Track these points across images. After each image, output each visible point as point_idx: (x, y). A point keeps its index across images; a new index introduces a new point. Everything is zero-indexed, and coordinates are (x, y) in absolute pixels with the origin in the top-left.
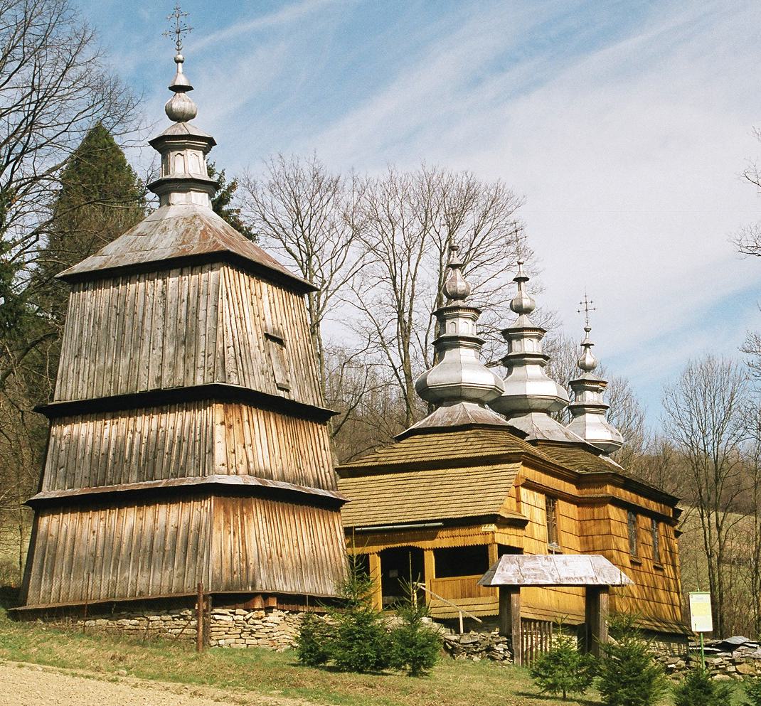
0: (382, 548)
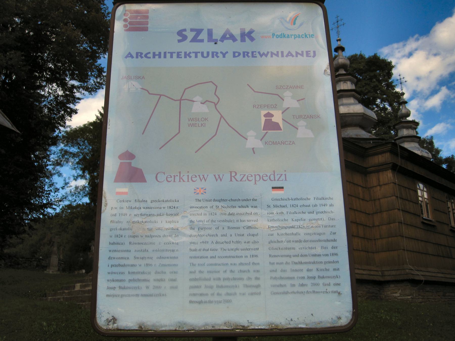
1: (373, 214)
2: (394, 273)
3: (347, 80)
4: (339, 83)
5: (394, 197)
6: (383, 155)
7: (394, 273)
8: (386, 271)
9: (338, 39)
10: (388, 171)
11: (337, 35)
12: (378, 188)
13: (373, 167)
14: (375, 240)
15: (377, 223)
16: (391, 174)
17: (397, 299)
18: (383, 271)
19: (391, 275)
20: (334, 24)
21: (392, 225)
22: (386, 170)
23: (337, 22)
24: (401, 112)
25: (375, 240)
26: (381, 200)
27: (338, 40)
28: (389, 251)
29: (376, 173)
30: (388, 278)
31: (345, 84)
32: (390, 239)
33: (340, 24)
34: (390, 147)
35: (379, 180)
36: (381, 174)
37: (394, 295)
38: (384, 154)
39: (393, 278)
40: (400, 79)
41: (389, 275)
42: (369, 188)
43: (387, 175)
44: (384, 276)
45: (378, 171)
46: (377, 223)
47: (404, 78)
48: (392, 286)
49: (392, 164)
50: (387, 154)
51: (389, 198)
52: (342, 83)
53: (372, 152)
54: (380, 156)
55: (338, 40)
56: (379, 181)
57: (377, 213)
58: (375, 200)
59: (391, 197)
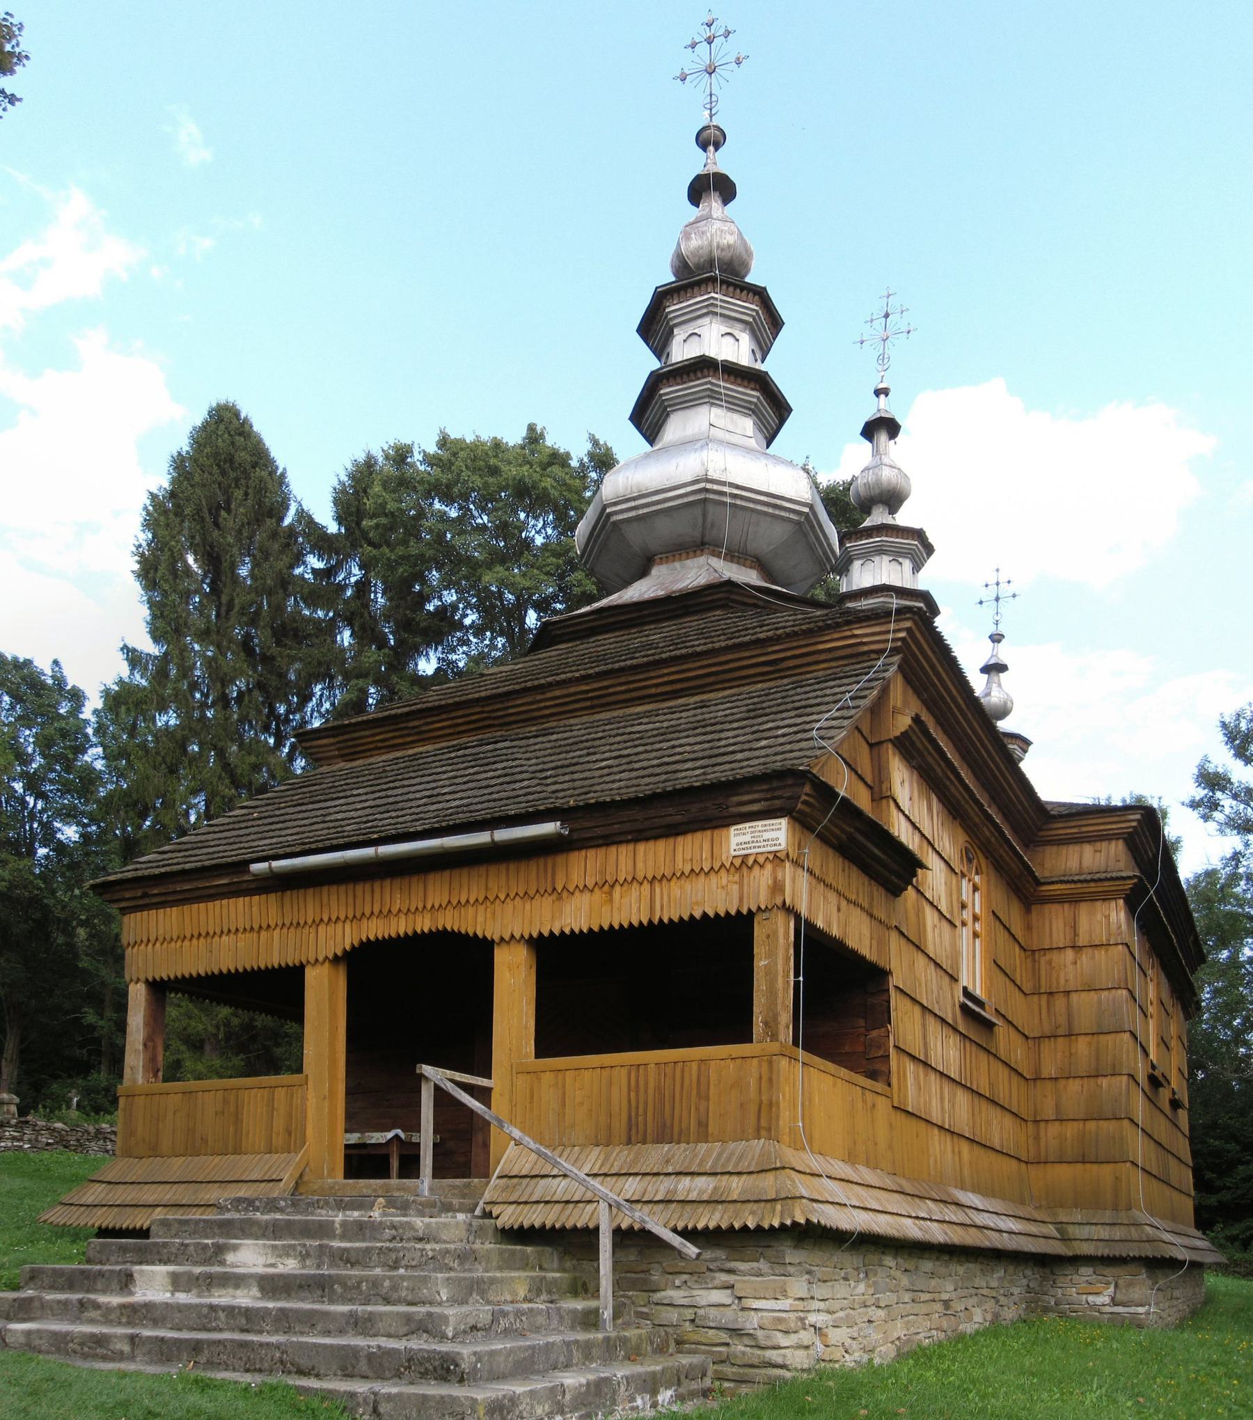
0: (347, 937)
1: (1039, 1038)
2: (1104, 1233)
3: (904, 555)
4: (877, 559)
5: (1125, 992)
6: (1098, 844)
7: (1104, 1233)
8: (1073, 1223)
9: (881, 386)
10: (1113, 904)
11: (880, 368)
12: (1070, 954)
13: (1061, 882)
14: (1036, 1122)
15: (1049, 1070)
16: (1122, 915)
17: (1099, 1311)
18: (1061, 1223)
19: (1092, 1240)
20: (872, 321)
21: (1104, 1082)
22: (1106, 897)
23: (887, 316)
24: (988, 698)
25: (1036, 1122)
26: (1074, 997)
27: (878, 393)
28: (1084, 1162)
29: (1066, 906)
30: (1086, 1249)
31: (895, 565)
32: (1091, 1125)
33: (896, 327)
34: (1134, 824)
35: (1075, 928)
36: (1084, 908)
37: (1091, 1298)
38: (1105, 844)
39: (1103, 1250)
40: (998, 584)
41: (1087, 1240)
42: (1033, 951)
43: (1108, 917)
44: (1070, 1240)
45: (1074, 900)
46: (1049, 1070)
47: (1009, 582)
48: (1086, 1271)
49: (1136, 880)
50: (1113, 843)
51: (1106, 993)
52: (886, 558)
53: (1061, 832)
54: (1088, 850)
55: (878, 393)
56: (1076, 934)
57: (1055, 1036)
58: (1051, 994)
59: (1113, 991)
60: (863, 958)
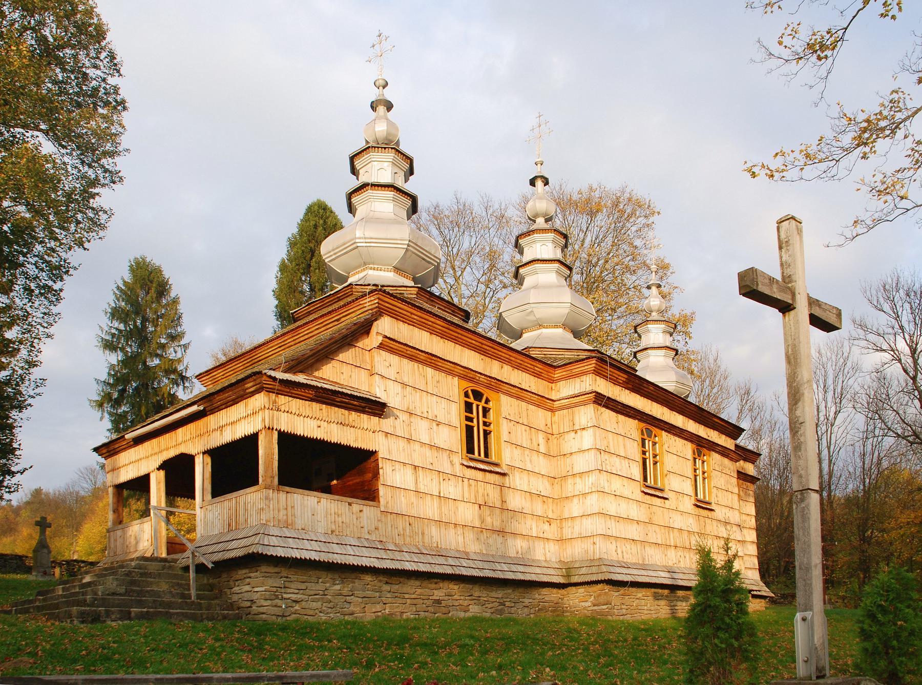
23: (540, 126)
60: (348, 448)
